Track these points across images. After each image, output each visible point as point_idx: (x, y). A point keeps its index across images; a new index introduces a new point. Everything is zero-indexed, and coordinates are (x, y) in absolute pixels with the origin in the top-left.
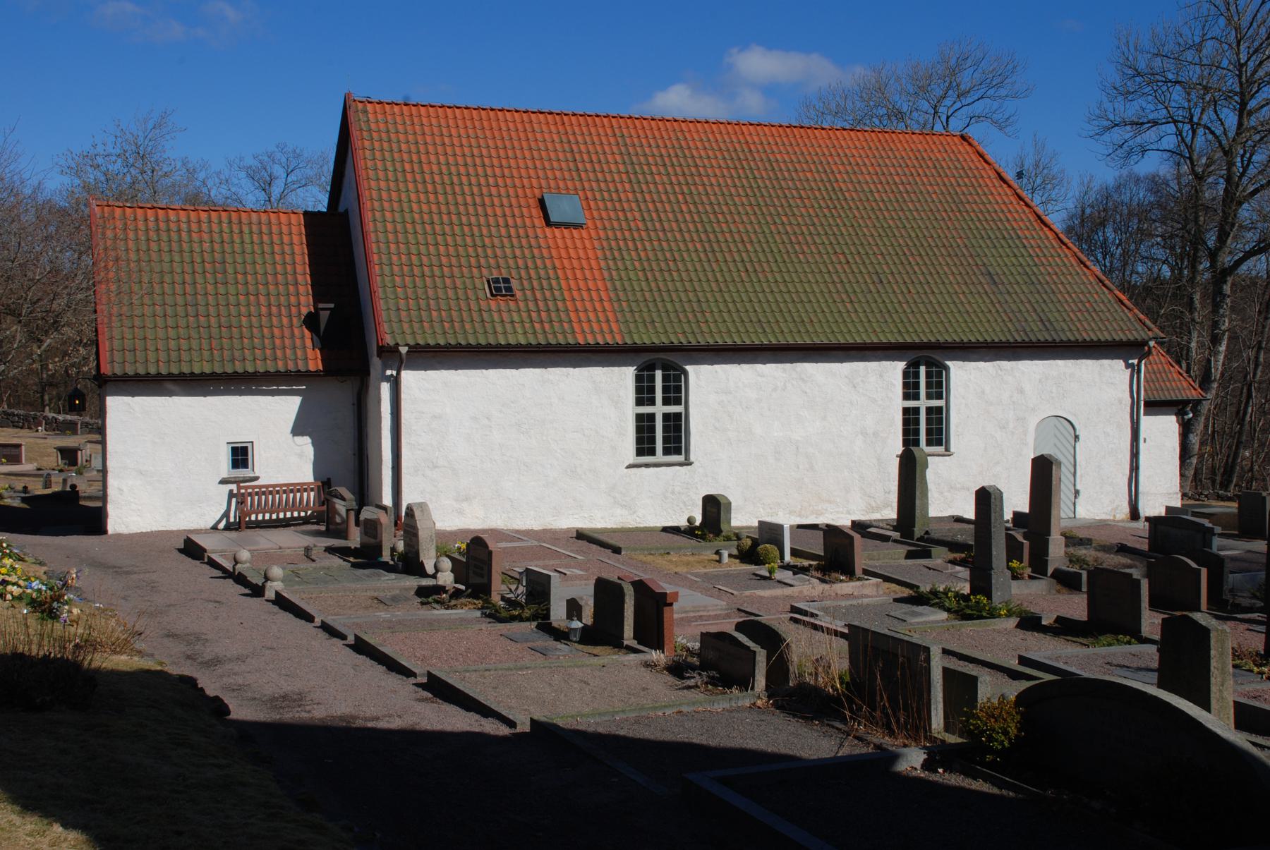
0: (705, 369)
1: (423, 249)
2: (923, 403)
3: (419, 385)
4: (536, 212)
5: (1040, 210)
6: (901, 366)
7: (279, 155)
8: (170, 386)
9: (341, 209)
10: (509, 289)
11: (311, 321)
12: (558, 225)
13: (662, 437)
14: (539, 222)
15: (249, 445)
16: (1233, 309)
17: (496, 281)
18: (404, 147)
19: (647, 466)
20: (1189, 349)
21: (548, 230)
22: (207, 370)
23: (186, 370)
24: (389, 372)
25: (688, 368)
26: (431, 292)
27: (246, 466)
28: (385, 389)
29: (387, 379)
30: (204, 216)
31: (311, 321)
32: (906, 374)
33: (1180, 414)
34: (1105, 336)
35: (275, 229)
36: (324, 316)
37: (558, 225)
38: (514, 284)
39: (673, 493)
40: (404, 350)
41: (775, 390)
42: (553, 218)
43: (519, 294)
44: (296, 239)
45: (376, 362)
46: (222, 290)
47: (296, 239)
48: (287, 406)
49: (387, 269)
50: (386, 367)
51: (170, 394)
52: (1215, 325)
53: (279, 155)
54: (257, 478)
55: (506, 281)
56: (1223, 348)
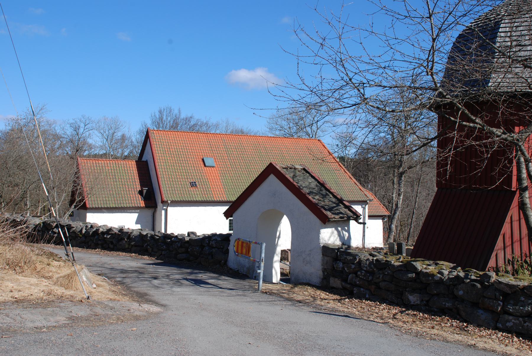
1: (172, 173)
3: (172, 211)
4: (202, 163)
5: (323, 188)
7: (83, 119)
8: (104, 210)
9: (144, 159)
10: (196, 185)
11: (141, 192)
12: (208, 167)
14: (203, 165)
16: (404, 185)
17: (192, 183)
18: (165, 144)
20: (393, 197)
22: (114, 206)
23: (109, 206)
26: (175, 186)
28: (163, 212)
29: (164, 209)
30: (108, 162)
31: (141, 192)
33: (383, 219)
34: (356, 199)
35: (128, 166)
36: (145, 192)
37: (208, 167)
38: (197, 183)
40: (169, 202)
42: (207, 165)
43: (198, 186)
44: (134, 169)
45: (160, 205)
46: (115, 184)
47: (134, 169)
49: (163, 179)
50: (164, 206)
51: (104, 212)
52: (399, 190)
53: (83, 119)
55: (195, 183)
56: (401, 197)
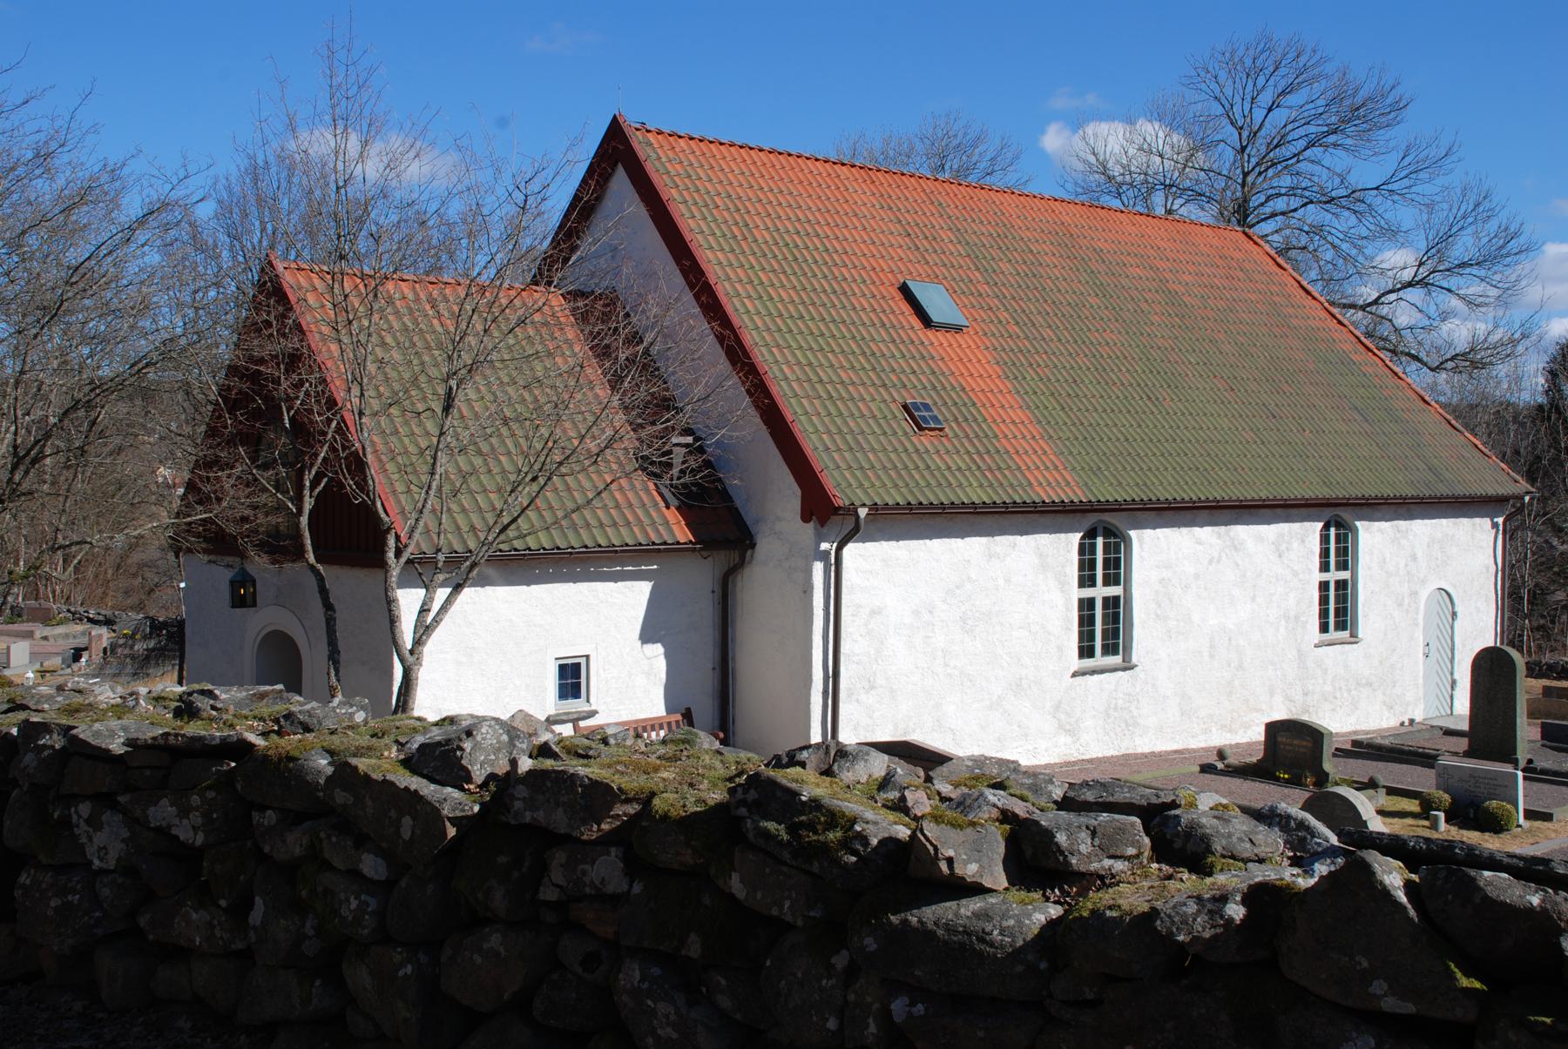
0: (1148, 533)
2: (1100, 592)
6: (1076, 537)
13: (1104, 631)
15: (583, 661)
19: (1093, 672)
21: (929, 333)
24: (824, 546)
25: (1133, 533)
27: (577, 695)
29: (824, 556)
32: (1082, 549)
39: (1116, 709)
41: (1210, 562)
48: (628, 599)
50: (820, 538)
54: (592, 714)
